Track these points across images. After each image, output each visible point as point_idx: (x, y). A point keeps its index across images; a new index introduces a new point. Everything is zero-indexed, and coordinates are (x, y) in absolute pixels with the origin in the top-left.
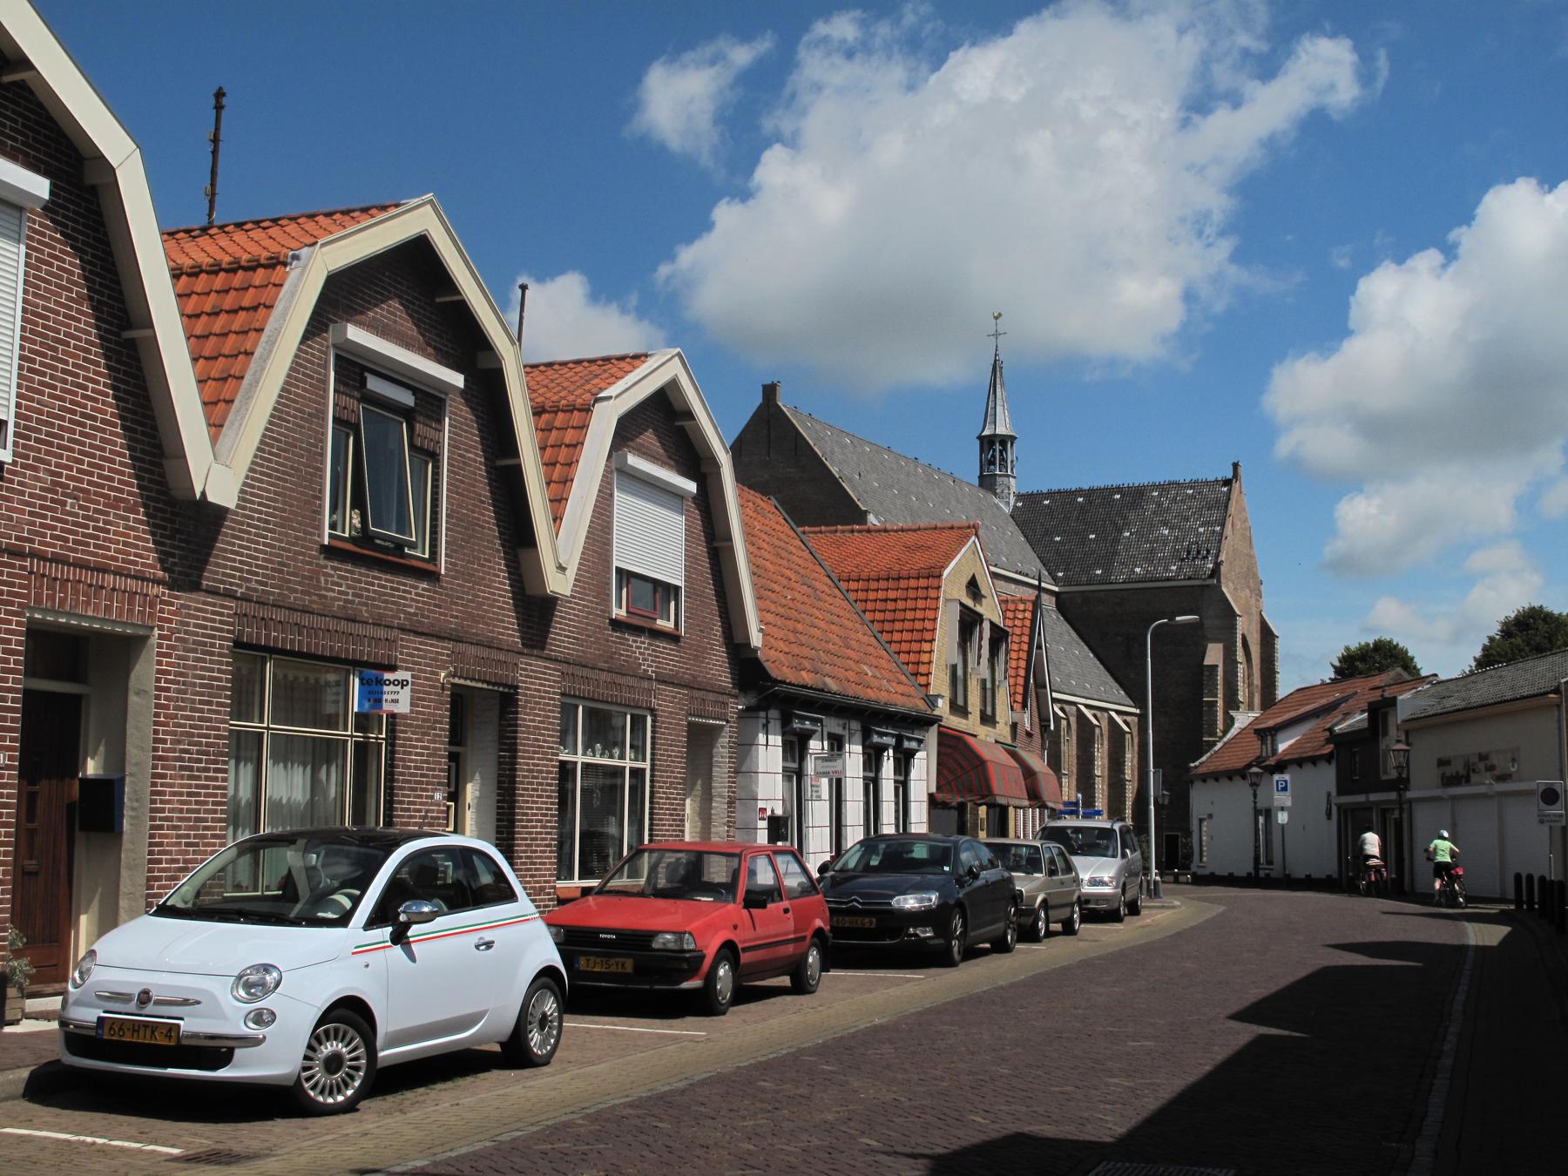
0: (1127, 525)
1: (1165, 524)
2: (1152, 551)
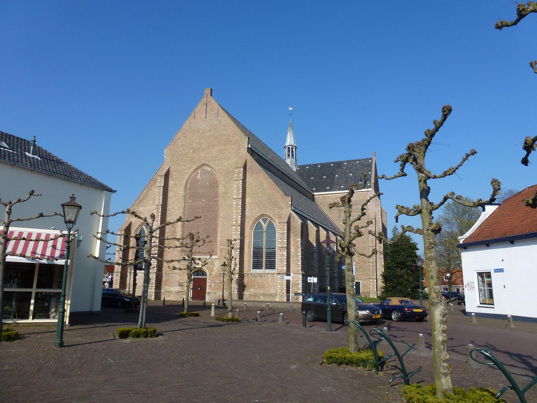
0: (337, 173)
1: (350, 173)
2: (347, 181)
